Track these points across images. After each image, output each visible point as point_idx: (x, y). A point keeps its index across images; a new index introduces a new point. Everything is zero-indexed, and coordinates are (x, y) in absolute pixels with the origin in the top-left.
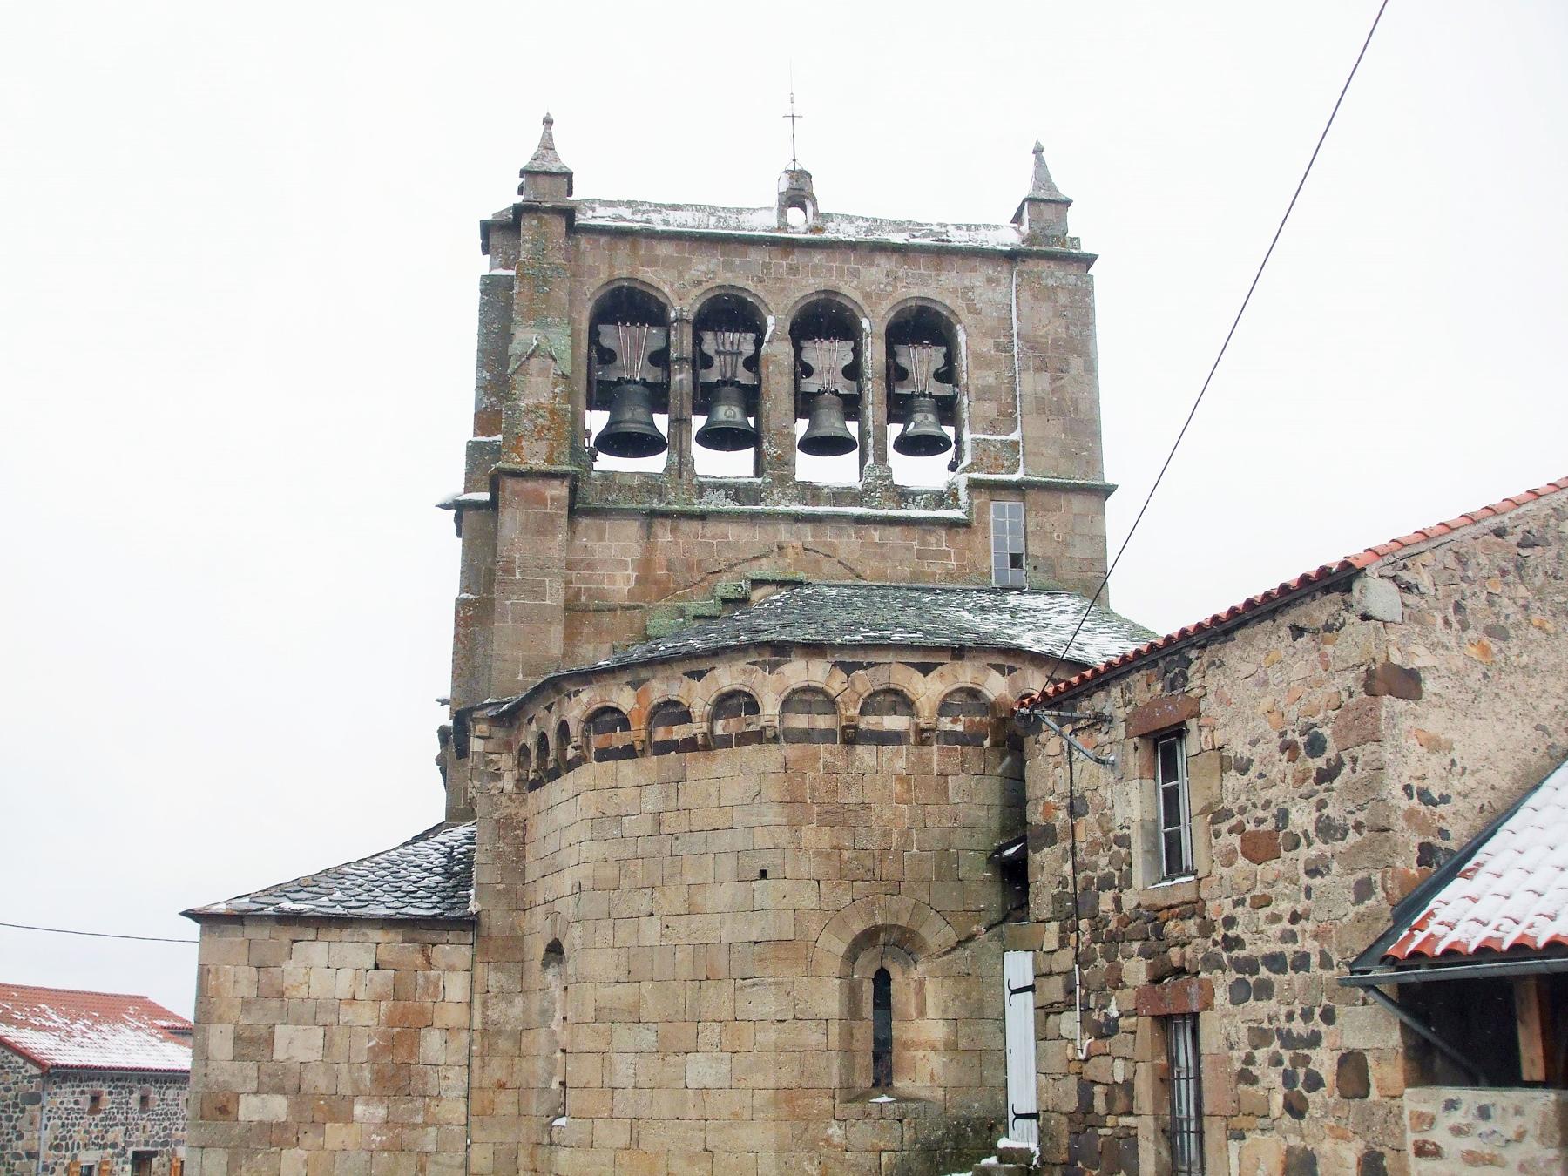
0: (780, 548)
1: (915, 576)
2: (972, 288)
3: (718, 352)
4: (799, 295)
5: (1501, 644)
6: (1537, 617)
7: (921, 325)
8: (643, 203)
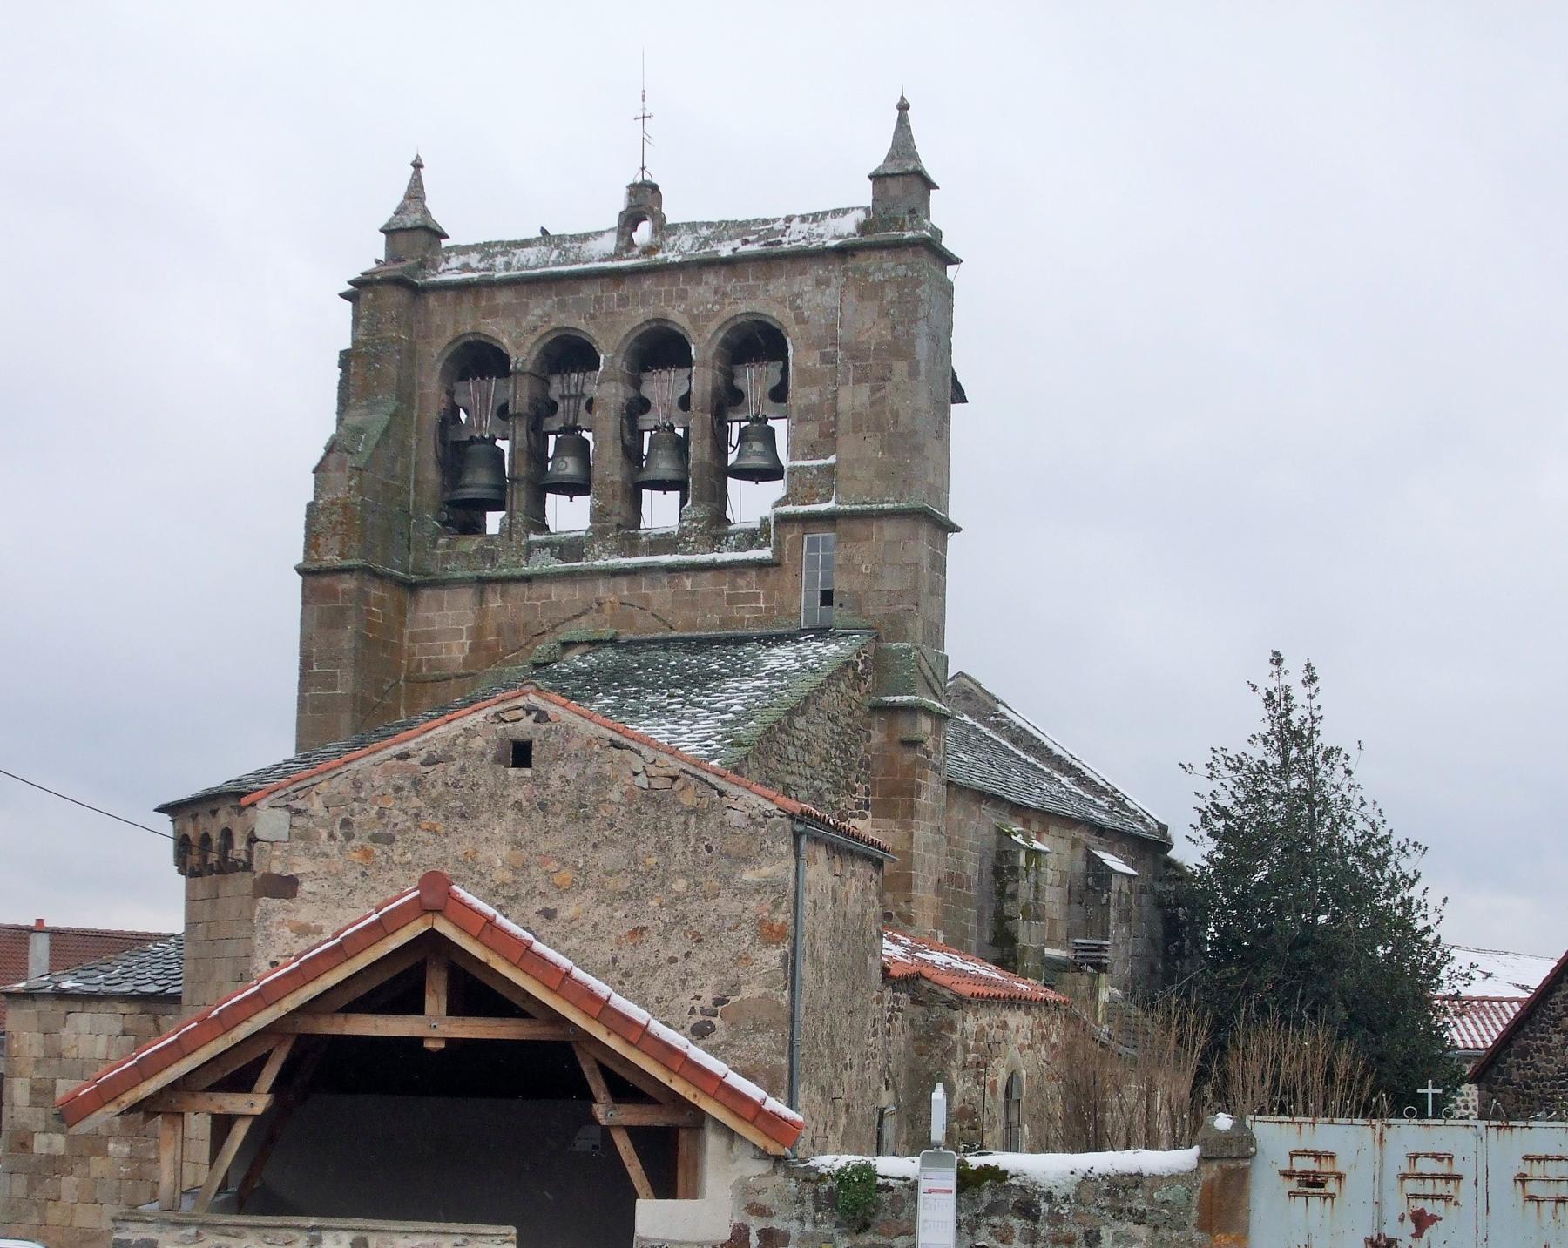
0: (600, 604)
1: (724, 623)
2: (800, 295)
3: (562, 397)
4: (628, 328)
5: (386, 848)
6: (427, 821)
7: (758, 342)
8: (496, 244)
